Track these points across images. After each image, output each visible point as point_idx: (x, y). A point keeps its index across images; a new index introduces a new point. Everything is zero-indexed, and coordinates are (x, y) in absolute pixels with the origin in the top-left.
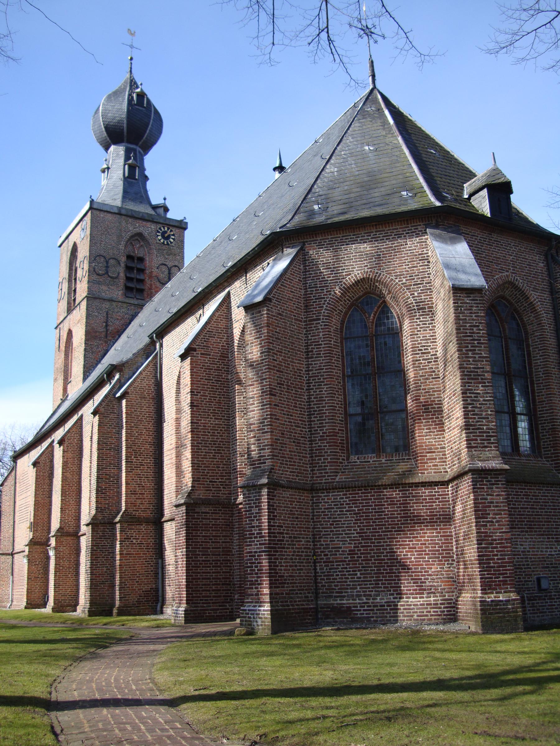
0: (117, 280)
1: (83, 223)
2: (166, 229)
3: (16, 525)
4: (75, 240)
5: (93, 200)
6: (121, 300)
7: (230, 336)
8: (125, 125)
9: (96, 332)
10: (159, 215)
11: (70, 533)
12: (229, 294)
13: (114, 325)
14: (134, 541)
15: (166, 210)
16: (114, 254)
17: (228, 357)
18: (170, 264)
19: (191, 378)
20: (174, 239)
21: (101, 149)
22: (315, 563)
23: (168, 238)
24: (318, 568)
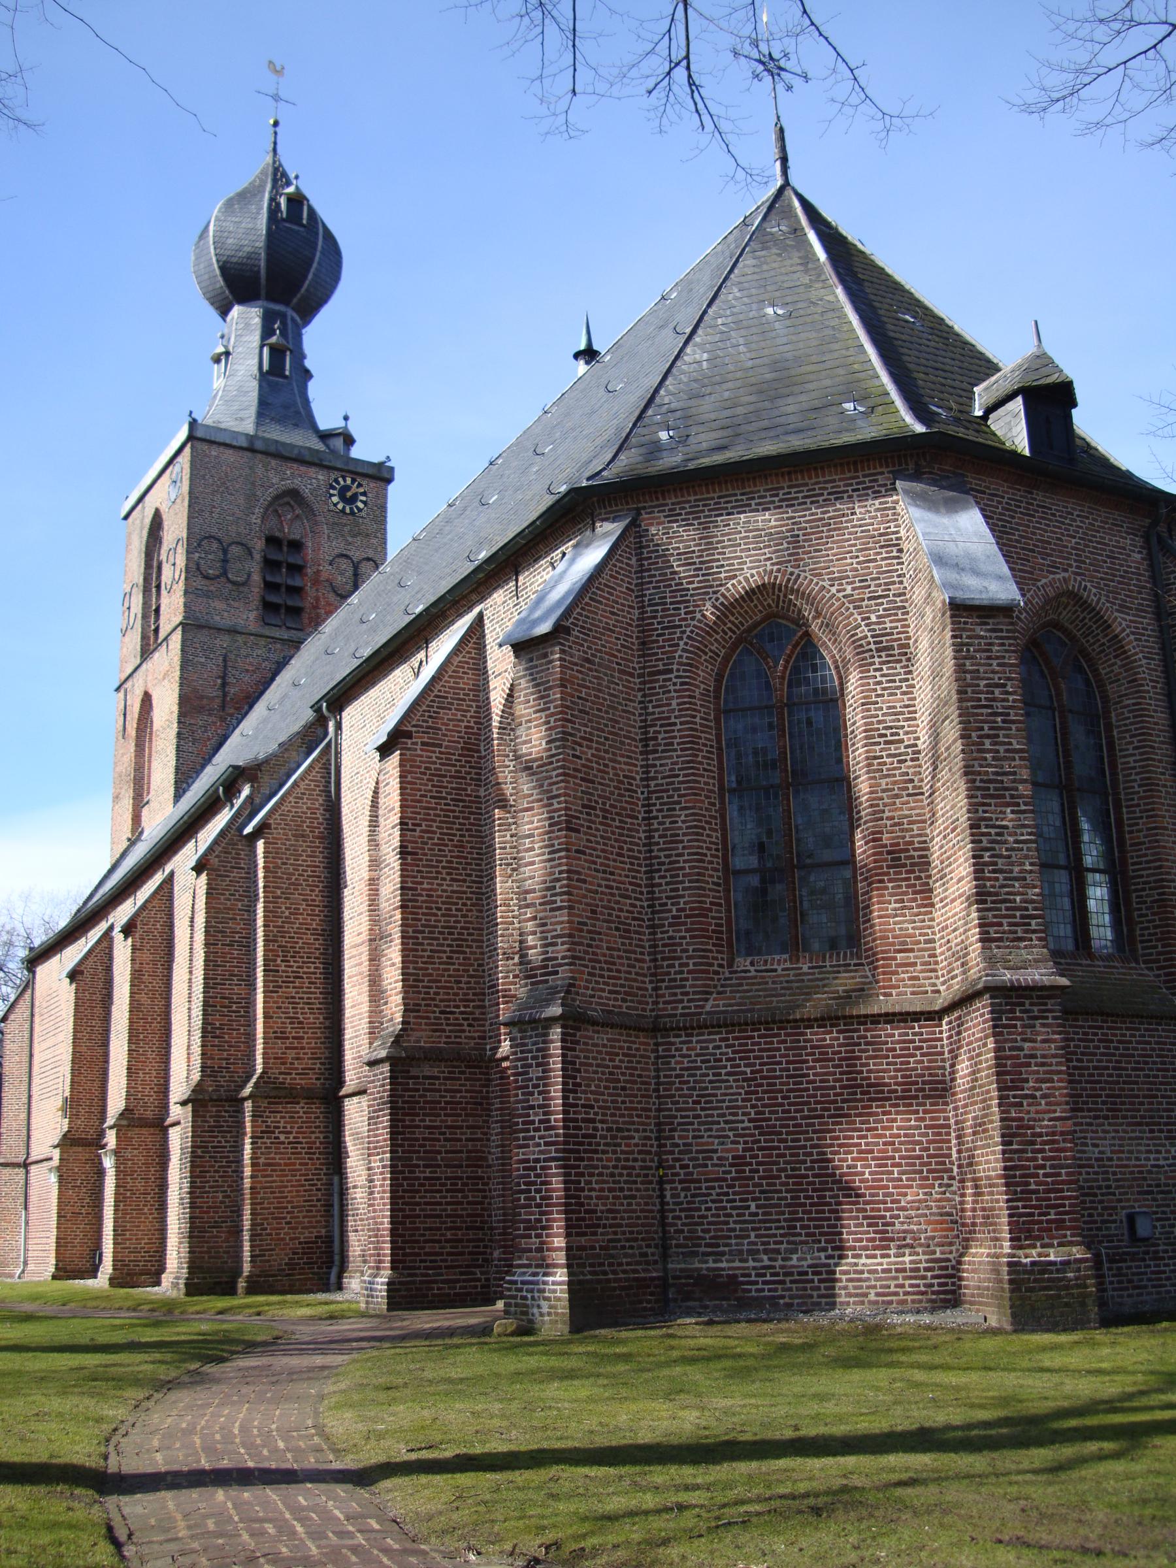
0: (245, 589)
1: (175, 469)
2: (349, 481)
3: (34, 1104)
4: (158, 505)
5: (195, 420)
6: (253, 631)
7: (484, 706)
8: (263, 264)
9: (202, 698)
10: (333, 452)
11: (146, 1120)
12: (480, 618)
13: (240, 683)
14: (282, 1137)
15: (349, 441)
16: (239, 534)
17: (479, 751)
18: (357, 555)
19: (401, 794)
20: (365, 503)
21: (212, 314)
22: (661, 1182)
23: (353, 499)
24: (668, 1194)
